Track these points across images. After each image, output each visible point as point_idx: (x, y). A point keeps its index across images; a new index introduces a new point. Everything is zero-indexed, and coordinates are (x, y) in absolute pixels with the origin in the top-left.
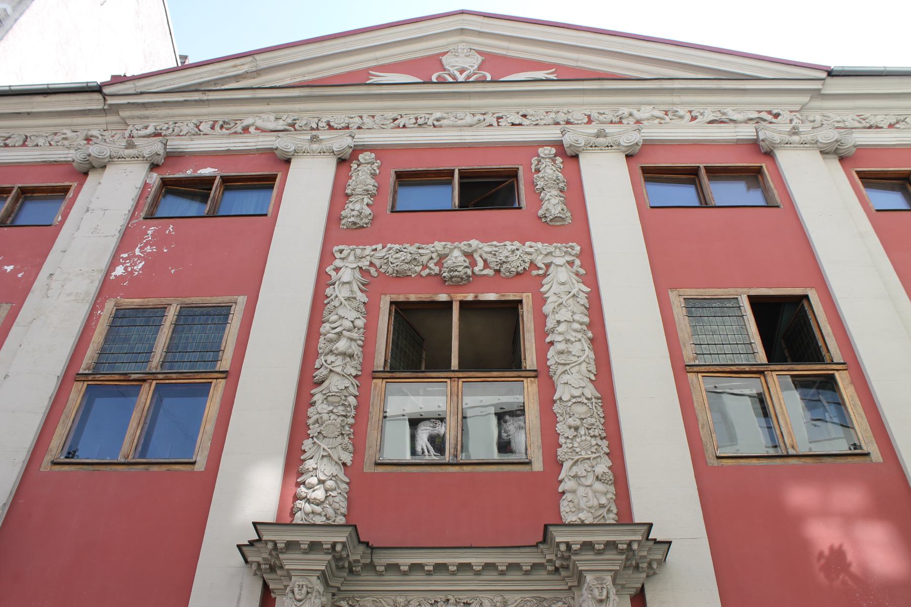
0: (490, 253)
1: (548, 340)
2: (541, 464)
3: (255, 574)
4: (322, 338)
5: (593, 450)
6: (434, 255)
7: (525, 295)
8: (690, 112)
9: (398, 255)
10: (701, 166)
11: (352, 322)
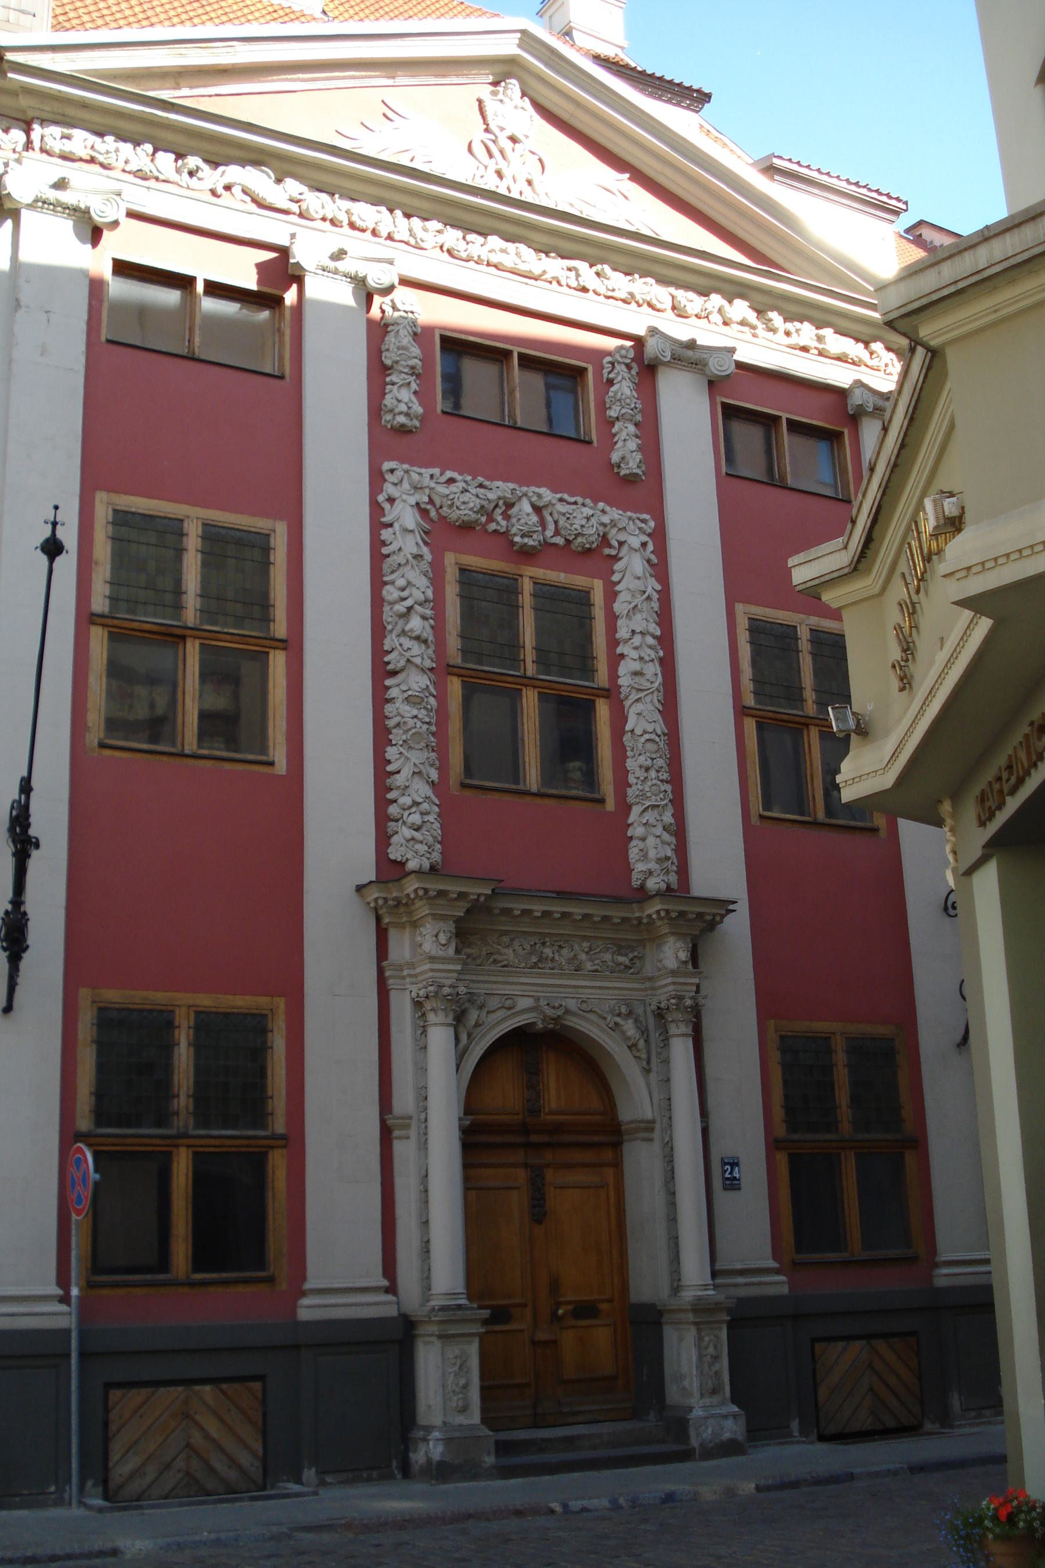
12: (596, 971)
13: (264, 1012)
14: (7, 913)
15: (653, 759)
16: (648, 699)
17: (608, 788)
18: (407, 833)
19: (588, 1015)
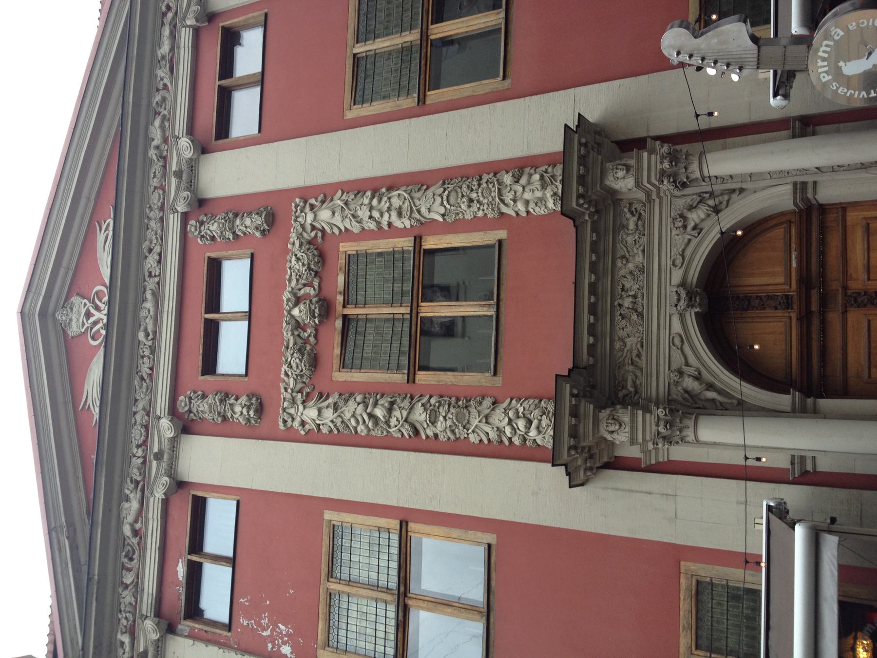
0: (298, 280)
1: (386, 228)
2: (501, 231)
3: (594, 474)
4: (373, 433)
5: (491, 186)
6: (296, 333)
7: (341, 249)
8: (158, 90)
9: (294, 366)
10: (218, 83)
11: (359, 404)
12: (643, 251)
13: (694, 583)
14: (791, 87)
15: (463, 196)
16: (417, 202)
17: (489, 237)
18: (533, 433)
19: (687, 259)
